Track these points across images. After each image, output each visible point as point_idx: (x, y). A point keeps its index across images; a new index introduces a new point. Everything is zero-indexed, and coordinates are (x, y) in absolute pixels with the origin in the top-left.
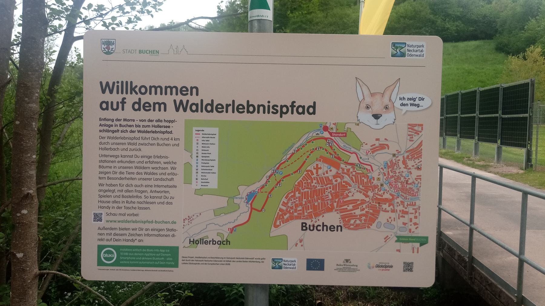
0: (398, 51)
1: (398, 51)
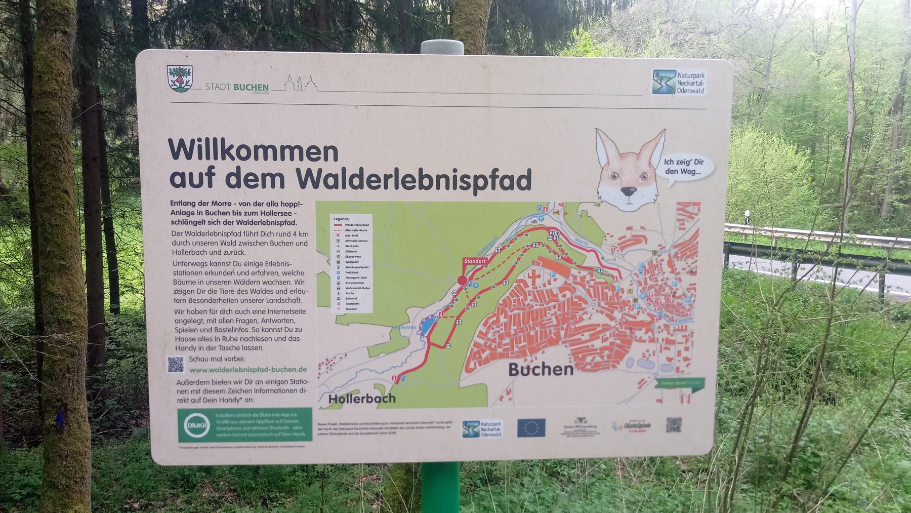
0: (663, 83)
1: (663, 83)
